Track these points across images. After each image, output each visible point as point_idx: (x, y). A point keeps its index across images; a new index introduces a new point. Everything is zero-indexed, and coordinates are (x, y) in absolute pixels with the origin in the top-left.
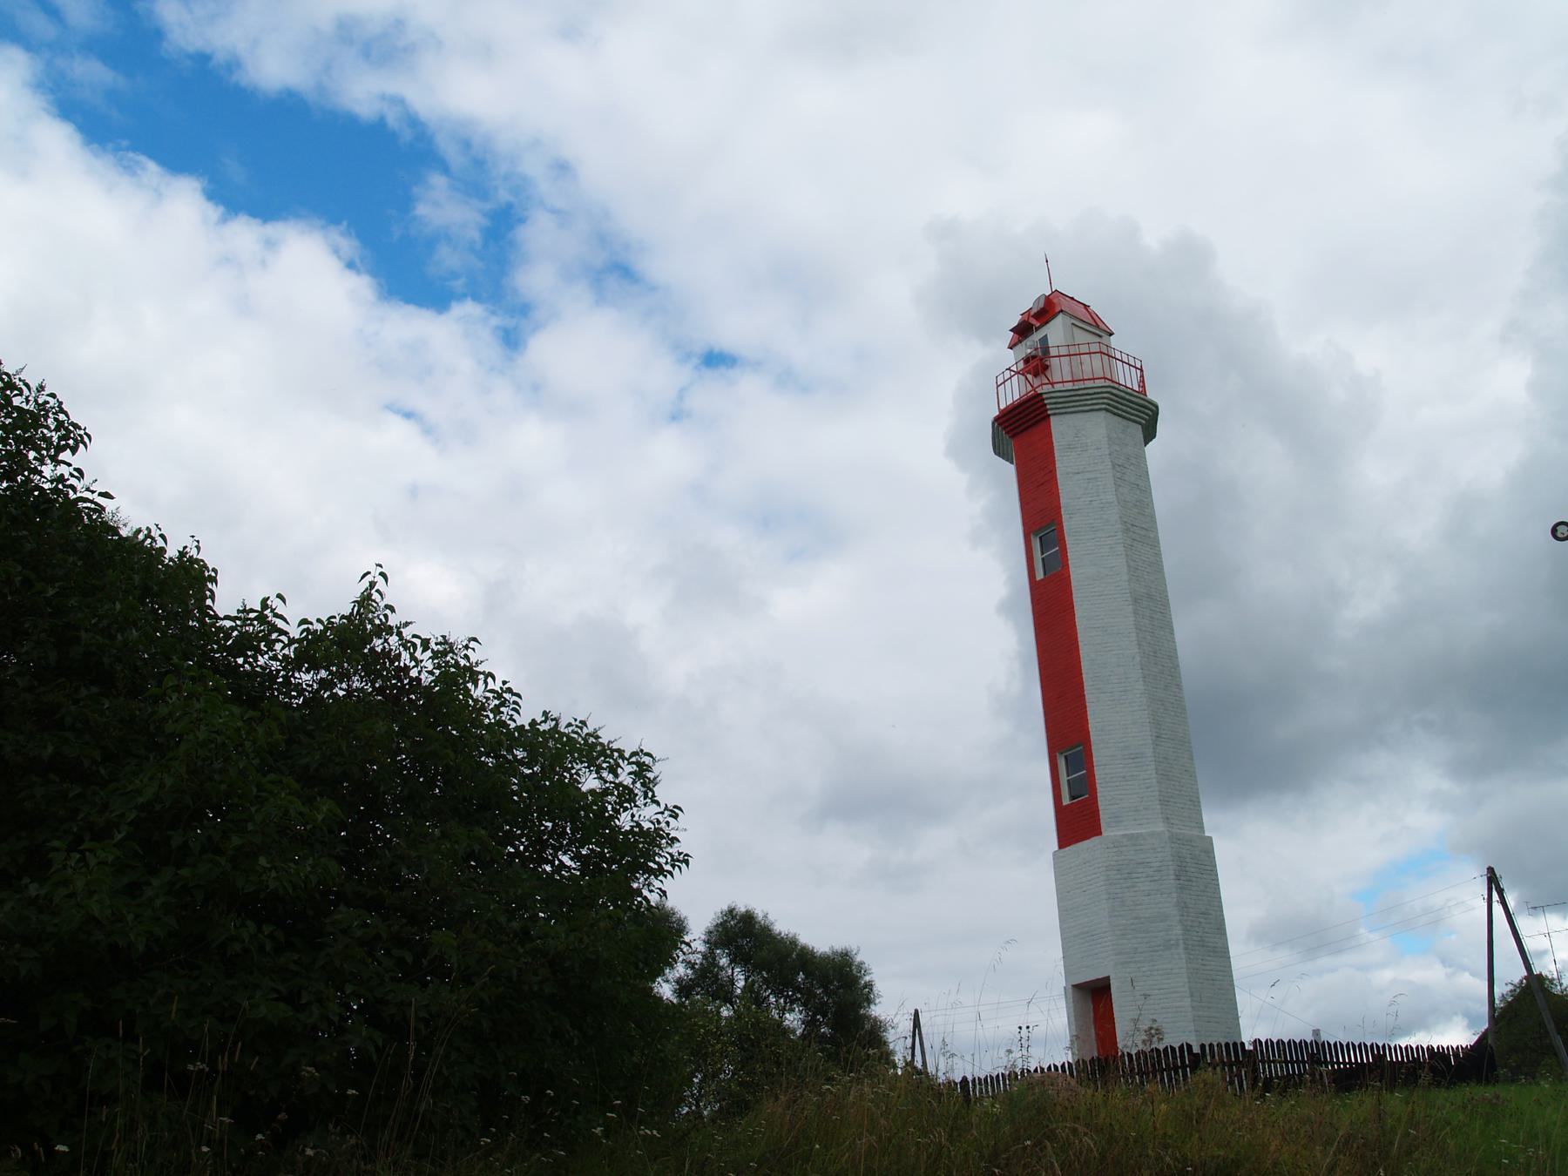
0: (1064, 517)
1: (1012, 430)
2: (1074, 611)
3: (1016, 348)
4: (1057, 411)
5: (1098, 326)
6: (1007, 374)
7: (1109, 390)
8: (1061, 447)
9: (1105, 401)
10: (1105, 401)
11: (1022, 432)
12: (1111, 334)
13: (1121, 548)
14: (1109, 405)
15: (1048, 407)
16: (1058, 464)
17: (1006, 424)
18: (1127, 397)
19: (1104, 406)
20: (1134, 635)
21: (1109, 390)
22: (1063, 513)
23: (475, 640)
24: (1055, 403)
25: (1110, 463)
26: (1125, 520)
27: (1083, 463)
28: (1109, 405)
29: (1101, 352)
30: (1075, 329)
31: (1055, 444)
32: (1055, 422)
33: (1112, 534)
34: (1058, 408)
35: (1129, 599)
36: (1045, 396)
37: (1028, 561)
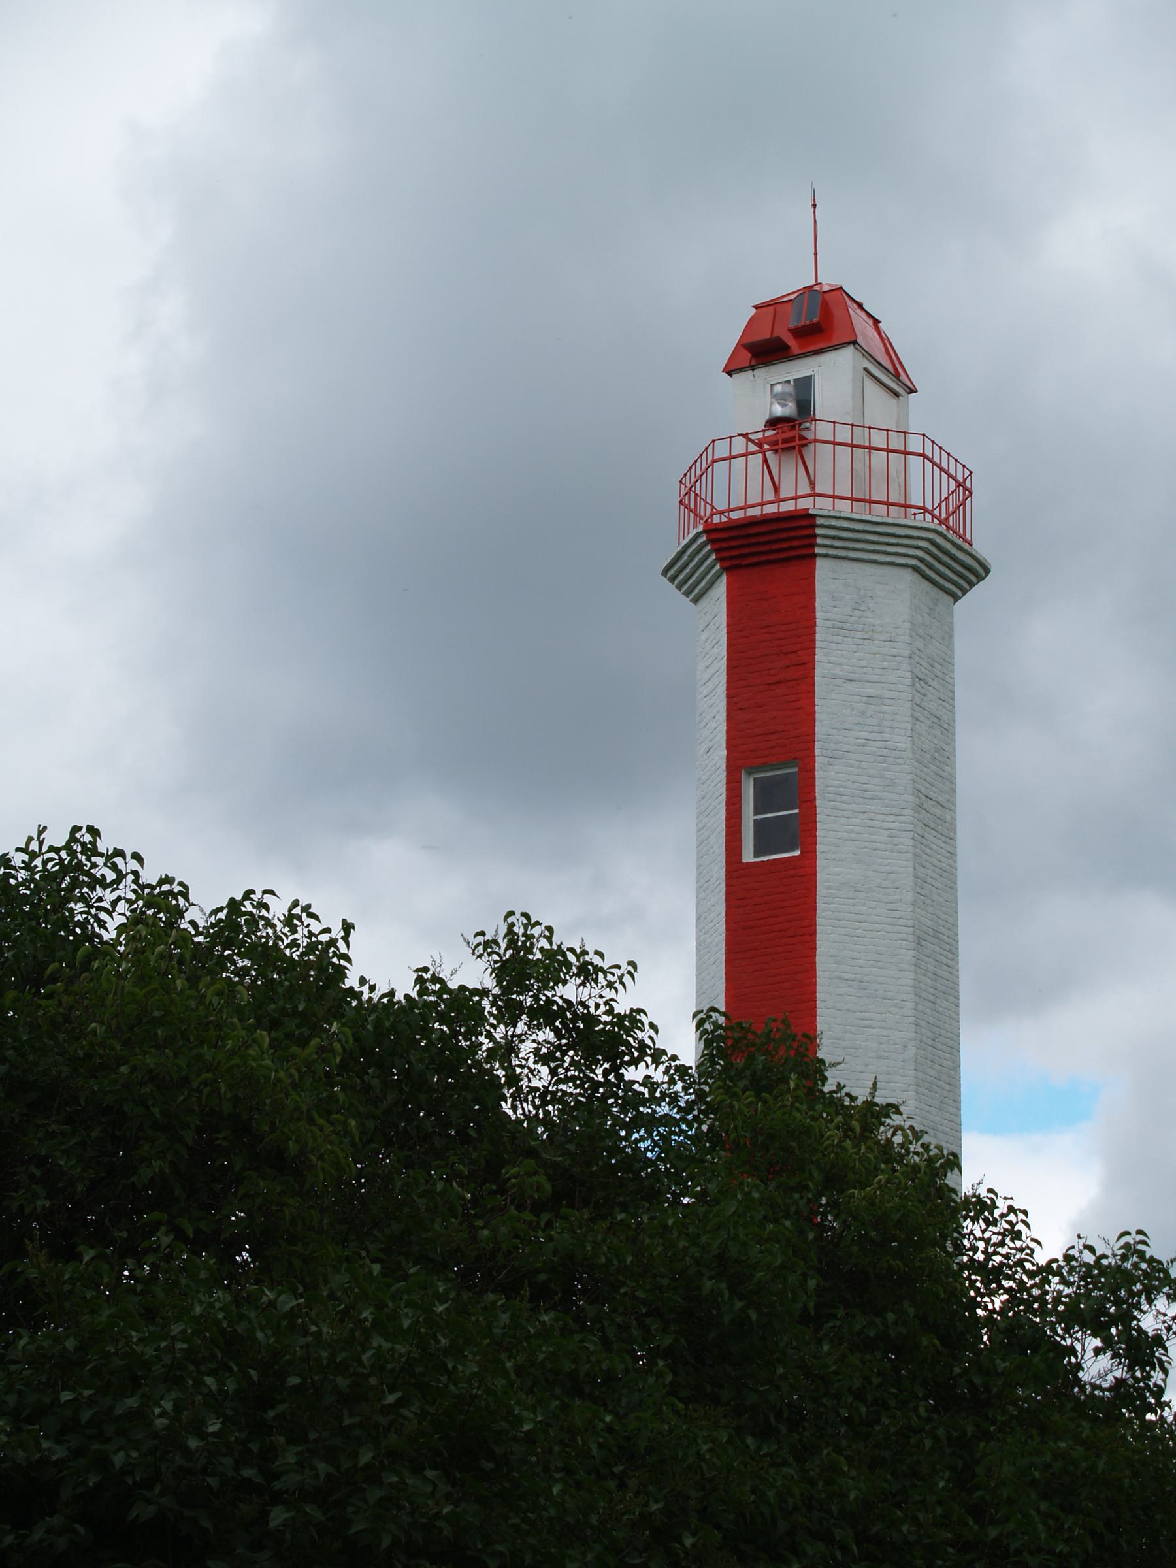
0: (819, 761)
1: (731, 558)
2: (814, 941)
3: (738, 377)
4: (832, 552)
5: (897, 376)
6: (739, 445)
7: (931, 536)
8: (829, 624)
9: (920, 553)
10: (920, 553)
11: (747, 566)
12: (912, 391)
13: (907, 841)
14: (921, 560)
15: (818, 531)
16: (819, 656)
17: (725, 545)
18: (954, 551)
19: (914, 562)
20: (911, 1005)
21: (931, 536)
22: (817, 752)
23: (271, 892)
24: (833, 538)
25: (908, 675)
26: (920, 787)
27: (863, 663)
28: (921, 560)
29: (923, 455)
30: (870, 384)
31: (818, 615)
32: (824, 570)
33: (894, 810)
34: (836, 548)
35: (911, 937)
36: (819, 521)
37: (728, 827)
